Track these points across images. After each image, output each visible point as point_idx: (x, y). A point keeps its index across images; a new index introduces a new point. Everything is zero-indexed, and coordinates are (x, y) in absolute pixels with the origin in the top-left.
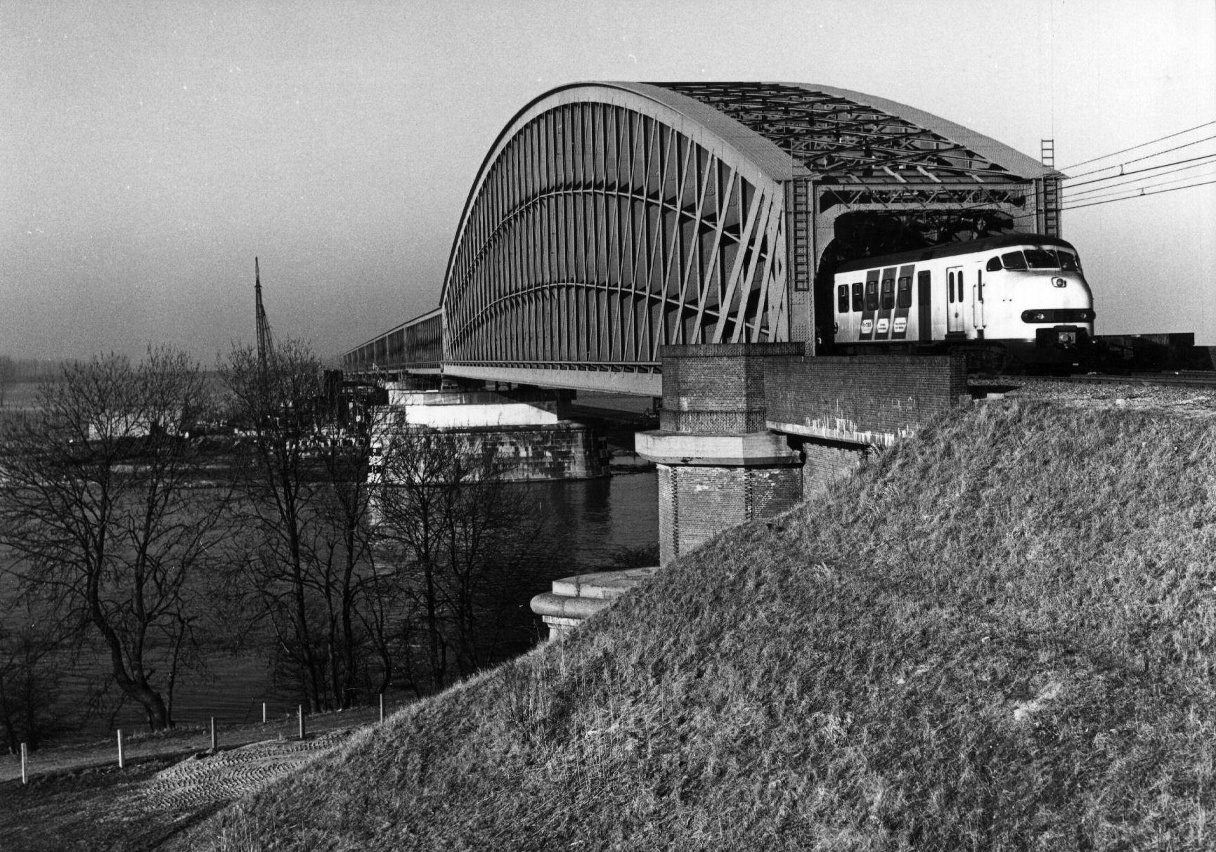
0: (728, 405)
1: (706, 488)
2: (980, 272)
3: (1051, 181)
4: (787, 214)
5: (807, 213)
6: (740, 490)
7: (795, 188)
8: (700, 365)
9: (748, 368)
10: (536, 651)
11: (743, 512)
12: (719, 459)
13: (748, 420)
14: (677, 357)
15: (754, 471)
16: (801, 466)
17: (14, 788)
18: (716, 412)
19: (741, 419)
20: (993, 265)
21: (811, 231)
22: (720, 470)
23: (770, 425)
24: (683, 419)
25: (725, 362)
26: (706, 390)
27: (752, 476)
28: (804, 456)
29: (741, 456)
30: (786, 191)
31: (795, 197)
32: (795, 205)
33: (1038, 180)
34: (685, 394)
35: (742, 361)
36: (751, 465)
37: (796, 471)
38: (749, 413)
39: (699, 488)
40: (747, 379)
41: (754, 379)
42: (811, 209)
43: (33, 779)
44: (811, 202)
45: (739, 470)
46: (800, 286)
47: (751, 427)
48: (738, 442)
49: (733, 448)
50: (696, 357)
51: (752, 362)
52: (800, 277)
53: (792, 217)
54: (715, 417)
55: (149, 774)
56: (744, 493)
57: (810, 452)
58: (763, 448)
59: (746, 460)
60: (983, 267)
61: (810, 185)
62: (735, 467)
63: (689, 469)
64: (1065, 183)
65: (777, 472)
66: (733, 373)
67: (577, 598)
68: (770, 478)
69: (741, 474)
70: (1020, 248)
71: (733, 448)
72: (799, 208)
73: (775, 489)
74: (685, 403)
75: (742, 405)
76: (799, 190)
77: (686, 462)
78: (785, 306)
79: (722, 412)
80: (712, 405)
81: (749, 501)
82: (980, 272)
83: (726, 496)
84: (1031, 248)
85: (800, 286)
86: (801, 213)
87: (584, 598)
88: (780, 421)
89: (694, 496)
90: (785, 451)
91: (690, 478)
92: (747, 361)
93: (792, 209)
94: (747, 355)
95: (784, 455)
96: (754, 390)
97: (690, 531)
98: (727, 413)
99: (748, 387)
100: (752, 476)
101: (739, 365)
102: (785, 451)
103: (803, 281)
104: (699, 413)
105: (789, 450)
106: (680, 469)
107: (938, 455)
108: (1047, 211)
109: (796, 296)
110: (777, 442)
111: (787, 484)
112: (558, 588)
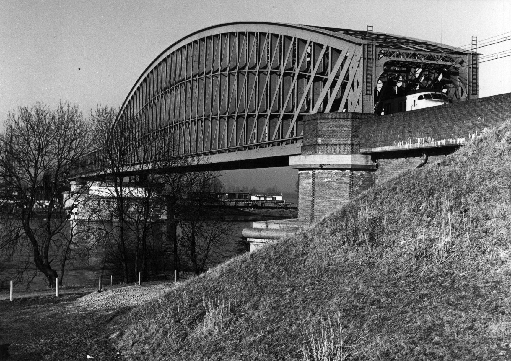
0: (342, 141)
1: (329, 179)
2: (415, 101)
3: (475, 56)
4: (364, 59)
5: (373, 59)
6: (347, 181)
7: (368, 47)
8: (329, 123)
9: (353, 124)
10: (453, 154)
11: (348, 191)
12: (339, 165)
13: (352, 148)
14: (316, 119)
15: (354, 172)
16: (375, 170)
17: (6, 303)
18: (336, 145)
19: (349, 148)
20: (420, 98)
21: (374, 68)
22: (337, 171)
23: (362, 150)
24: (319, 147)
25: (341, 121)
26: (332, 134)
27: (353, 174)
28: (377, 166)
29: (351, 164)
30: (364, 49)
31: (368, 51)
32: (368, 55)
33: (470, 54)
34: (320, 136)
35: (350, 121)
36: (354, 168)
37: (372, 173)
38: (352, 145)
39: (326, 180)
40: (352, 129)
41: (355, 129)
42: (374, 57)
43: (15, 300)
44: (374, 55)
45: (347, 171)
46: (368, 92)
47: (353, 152)
48: (350, 157)
49: (347, 160)
50: (328, 119)
51: (355, 121)
52: (368, 89)
53: (366, 61)
54: (335, 147)
55: (74, 299)
56: (349, 182)
57: (381, 164)
58: (361, 160)
59: (353, 165)
60: (416, 99)
61: (374, 47)
62: (343, 169)
63: (321, 171)
64: (480, 56)
65: (364, 173)
66: (345, 128)
67: (267, 229)
68: (361, 175)
69: (348, 173)
70: (429, 93)
71: (347, 160)
72: (369, 57)
73: (363, 181)
74: (320, 140)
75: (349, 141)
76: (369, 49)
77: (321, 167)
78: (361, 102)
79: (339, 144)
80: (334, 141)
81: (351, 185)
82: (415, 101)
83: (340, 183)
84: (434, 93)
85: (368, 92)
86: (370, 59)
87: (270, 229)
88: (371, 147)
89: (323, 183)
90: (370, 163)
91: (322, 174)
92: (353, 121)
93: (366, 57)
94: (353, 118)
95: (369, 164)
96: (355, 134)
97: (320, 199)
98: (342, 145)
99: (352, 133)
100: (353, 174)
101: (349, 122)
102: (370, 163)
103: (369, 91)
104: (328, 145)
105: (372, 162)
106: (316, 171)
107: (461, 155)
108: (473, 68)
109: (366, 97)
110: (367, 158)
111: (368, 179)
112: (255, 225)
